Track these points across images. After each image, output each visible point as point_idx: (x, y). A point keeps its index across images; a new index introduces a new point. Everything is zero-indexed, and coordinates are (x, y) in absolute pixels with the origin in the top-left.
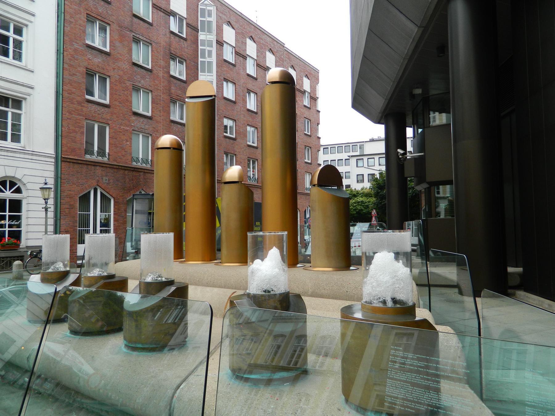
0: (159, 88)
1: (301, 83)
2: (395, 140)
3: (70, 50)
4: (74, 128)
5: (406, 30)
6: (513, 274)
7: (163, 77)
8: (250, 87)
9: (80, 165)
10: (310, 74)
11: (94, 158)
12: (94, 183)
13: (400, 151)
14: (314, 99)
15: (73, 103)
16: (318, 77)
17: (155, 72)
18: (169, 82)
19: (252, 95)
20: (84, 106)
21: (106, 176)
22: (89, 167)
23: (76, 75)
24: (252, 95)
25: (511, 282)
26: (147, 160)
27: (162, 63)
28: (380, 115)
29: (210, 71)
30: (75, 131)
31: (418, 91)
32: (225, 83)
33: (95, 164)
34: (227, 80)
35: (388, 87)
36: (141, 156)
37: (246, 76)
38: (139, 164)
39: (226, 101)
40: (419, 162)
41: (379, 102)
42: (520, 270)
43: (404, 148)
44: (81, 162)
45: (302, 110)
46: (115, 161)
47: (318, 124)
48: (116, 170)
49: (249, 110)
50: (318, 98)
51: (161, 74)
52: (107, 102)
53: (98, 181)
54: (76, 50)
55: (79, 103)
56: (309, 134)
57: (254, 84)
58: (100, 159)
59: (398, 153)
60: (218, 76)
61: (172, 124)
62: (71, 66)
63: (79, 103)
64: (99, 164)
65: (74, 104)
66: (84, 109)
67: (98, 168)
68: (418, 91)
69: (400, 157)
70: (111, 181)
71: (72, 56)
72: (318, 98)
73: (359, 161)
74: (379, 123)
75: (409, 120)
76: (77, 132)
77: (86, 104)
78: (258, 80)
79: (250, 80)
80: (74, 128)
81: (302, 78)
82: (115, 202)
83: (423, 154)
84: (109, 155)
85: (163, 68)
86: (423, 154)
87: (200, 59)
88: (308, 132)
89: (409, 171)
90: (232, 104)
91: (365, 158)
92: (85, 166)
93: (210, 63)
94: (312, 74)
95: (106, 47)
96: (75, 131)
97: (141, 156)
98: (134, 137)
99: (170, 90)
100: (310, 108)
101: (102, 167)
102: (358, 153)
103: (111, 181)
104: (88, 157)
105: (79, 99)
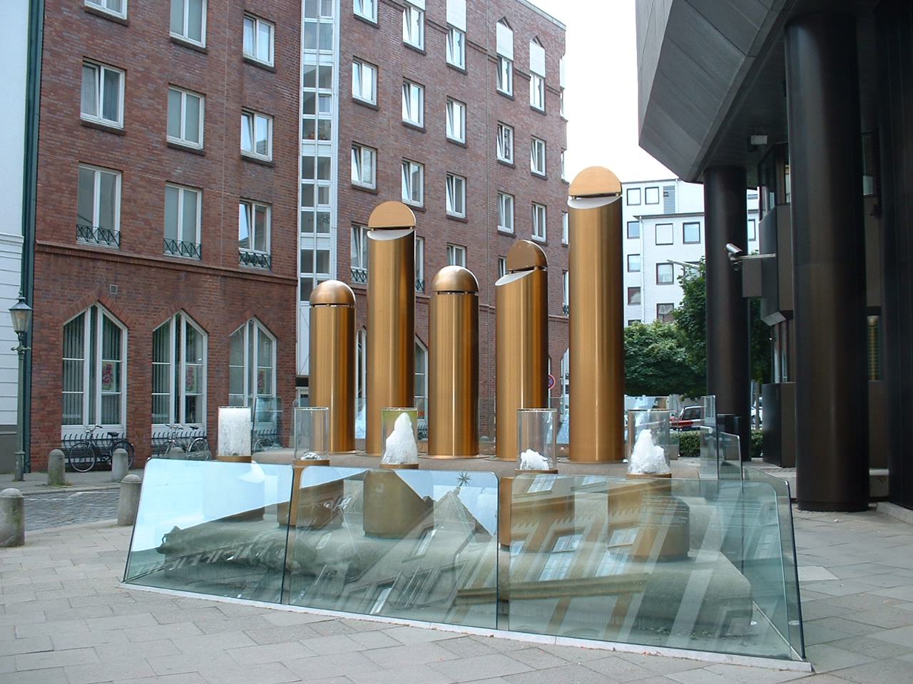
0: (220, 88)
1: (523, 55)
2: (724, 222)
3: (56, 24)
4: (57, 183)
5: (728, 59)
6: (879, 477)
7: (229, 62)
8: (410, 72)
9: (68, 260)
10: (545, 33)
11: (93, 244)
12: (93, 294)
13: (733, 249)
14: (553, 91)
15: (56, 131)
16: (564, 39)
17: (213, 53)
18: (241, 73)
19: (414, 89)
20: (77, 137)
21: (116, 281)
22: (84, 262)
23: (65, 73)
24: (414, 89)
25: (874, 492)
26: (110, 233)
27: (228, 34)
28: (696, 169)
29: (326, 44)
30: (59, 190)
31: (761, 140)
32: (355, 66)
33: (95, 256)
34: (360, 61)
35: (709, 128)
36: (180, 239)
37: (402, 49)
38: (177, 254)
39: (358, 108)
40: (767, 268)
41: (693, 150)
42: (885, 472)
43: (742, 242)
44: (70, 253)
45: (525, 118)
46: (131, 249)
47: (563, 150)
48: (133, 269)
49: (406, 125)
50: (562, 89)
51: (225, 58)
52: (119, 124)
53: (100, 293)
54: (66, 23)
55: (69, 130)
56: (543, 174)
57: (418, 65)
58: (104, 246)
59: (728, 251)
60: (342, 53)
61: (245, 164)
62: (54, 54)
63: (69, 130)
64: (103, 257)
65: (59, 132)
66: (79, 143)
67: (99, 264)
68: (761, 140)
69: (732, 259)
70: (124, 292)
71: (59, 34)
72: (562, 89)
73: (687, 227)
74: (694, 181)
75: (751, 177)
76: (63, 192)
77: (81, 132)
78: (429, 56)
79: (411, 58)
80: (57, 183)
81: (527, 44)
82: (130, 337)
83: (774, 255)
84: (120, 237)
85: (230, 44)
86: (774, 255)
87: (304, 20)
88: (508, 225)
89: (751, 287)
90: (371, 113)
91: (678, 223)
92: (77, 261)
93: (326, 28)
94: (551, 35)
95: (119, 10)
96: (59, 190)
97: (180, 239)
98: (168, 196)
99: (241, 90)
100: (544, 114)
101: (108, 261)
102: (659, 210)
103: (124, 292)
104: (82, 242)
105: (67, 121)
